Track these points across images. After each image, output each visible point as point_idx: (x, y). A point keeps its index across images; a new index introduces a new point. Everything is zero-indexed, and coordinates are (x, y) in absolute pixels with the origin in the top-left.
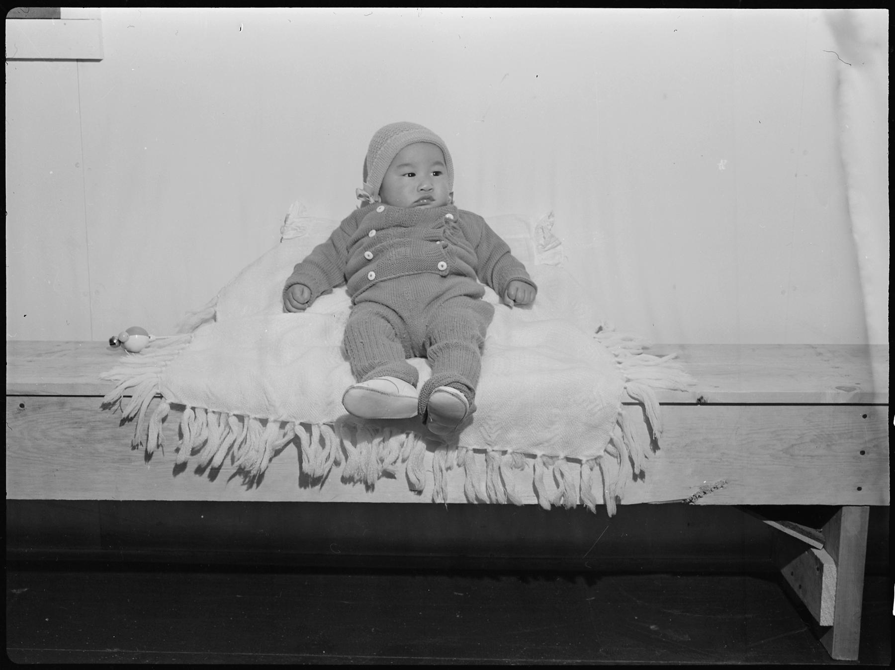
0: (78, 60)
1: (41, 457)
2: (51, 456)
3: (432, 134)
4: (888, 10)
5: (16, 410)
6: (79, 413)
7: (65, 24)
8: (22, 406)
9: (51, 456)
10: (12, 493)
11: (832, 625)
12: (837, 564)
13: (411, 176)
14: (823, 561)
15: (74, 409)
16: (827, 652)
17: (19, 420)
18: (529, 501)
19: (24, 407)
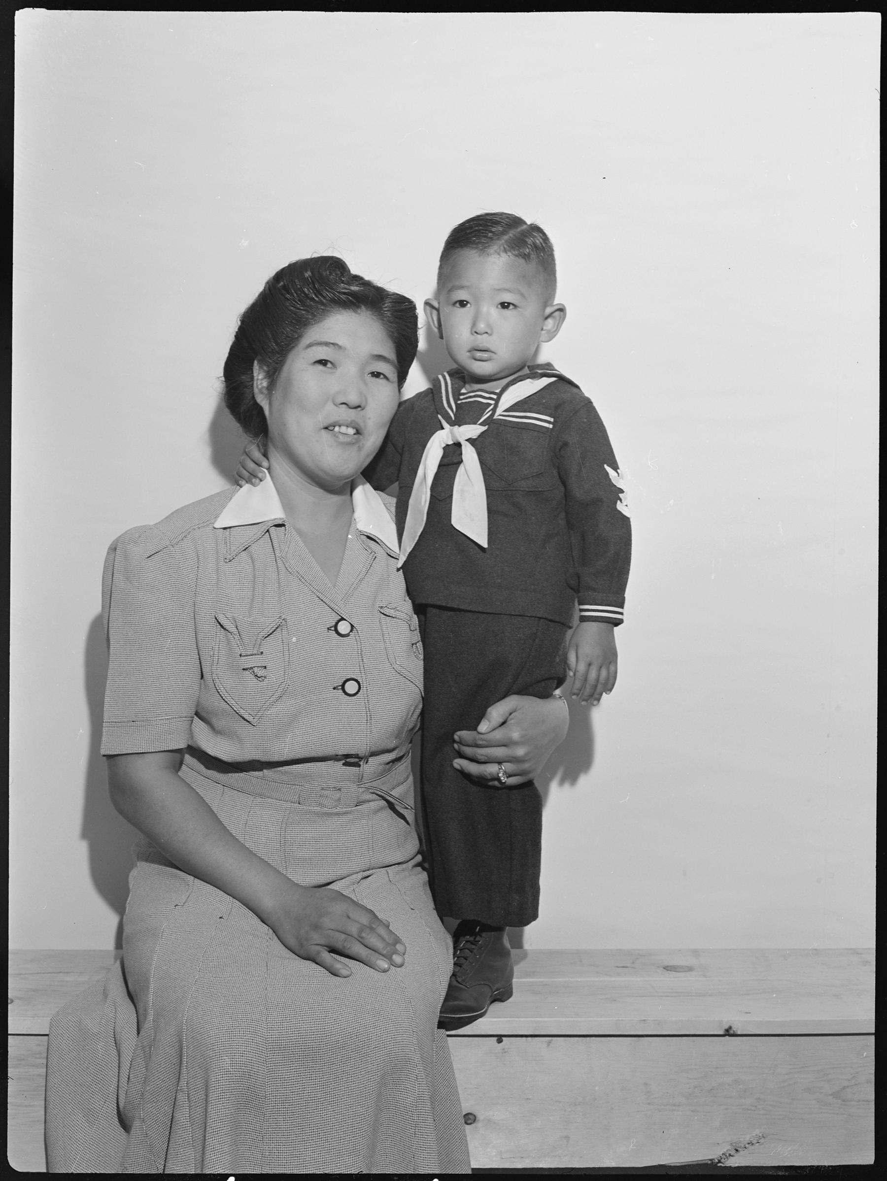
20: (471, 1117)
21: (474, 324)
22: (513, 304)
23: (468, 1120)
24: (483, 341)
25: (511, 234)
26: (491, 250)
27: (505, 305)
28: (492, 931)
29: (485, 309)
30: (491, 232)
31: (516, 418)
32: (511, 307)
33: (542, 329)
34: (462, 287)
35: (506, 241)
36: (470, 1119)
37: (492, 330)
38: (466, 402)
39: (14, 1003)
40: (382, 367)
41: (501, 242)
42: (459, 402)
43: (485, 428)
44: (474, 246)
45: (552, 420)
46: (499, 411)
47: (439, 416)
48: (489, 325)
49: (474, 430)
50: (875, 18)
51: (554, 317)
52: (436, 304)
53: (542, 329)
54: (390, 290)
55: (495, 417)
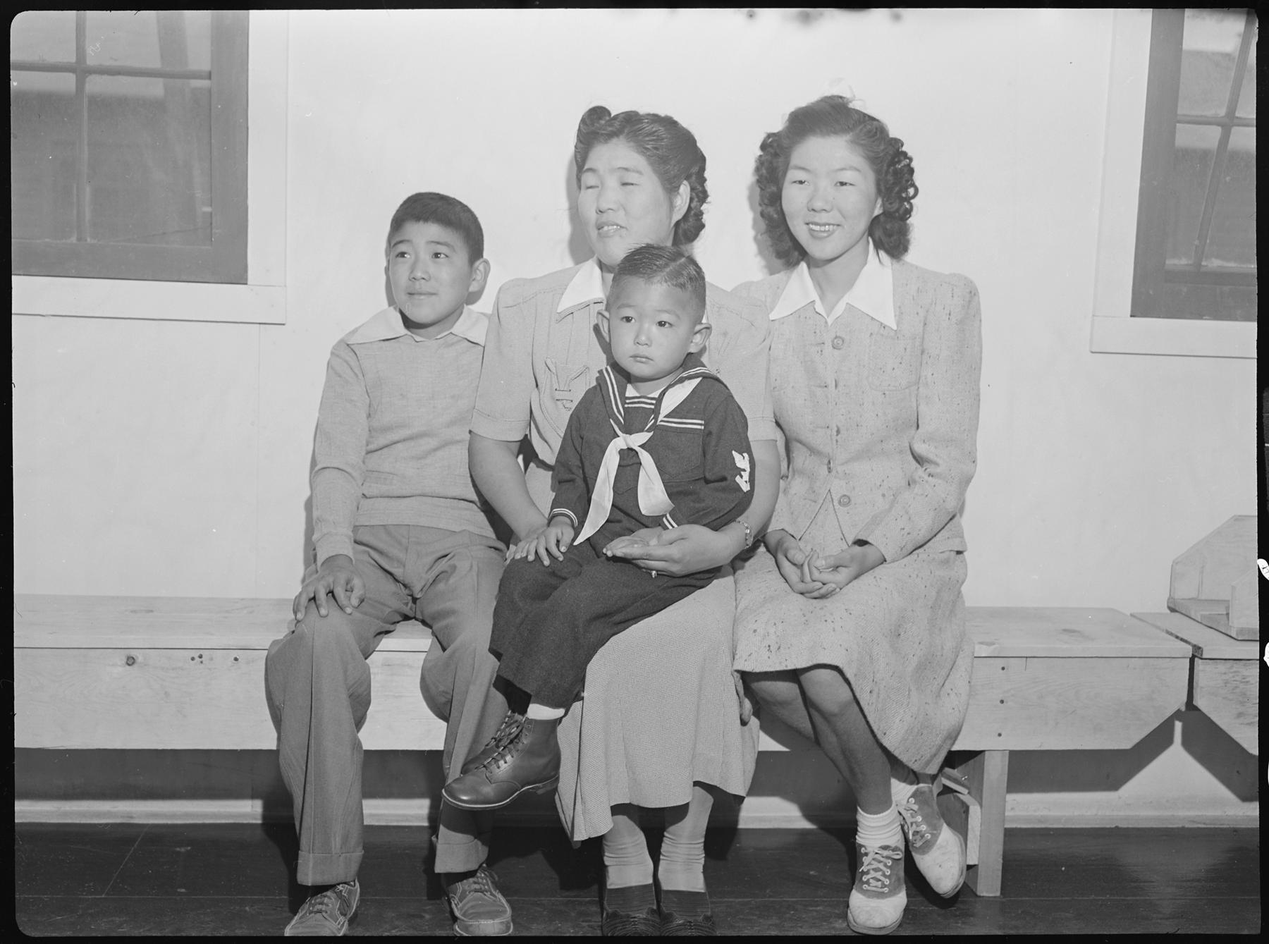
3: (393, 638)
4: (1257, 931)
11: (977, 863)
12: (981, 806)
14: (968, 804)
16: (972, 890)
21: (637, 337)
22: (669, 323)
24: (643, 350)
25: (673, 266)
26: (657, 279)
27: (661, 324)
28: (14, 898)
29: (646, 326)
30: (655, 265)
31: (675, 423)
32: (667, 325)
33: (692, 342)
34: (629, 306)
35: (667, 273)
37: (651, 343)
38: (632, 407)
41: (662, 274)
42: (626, 406)
43: (652, 433)
44: (642, 275)
45: (703, 422)
46: (661, 417)
47: (611, 421)
48: (649, 339)
49: (644, 437)
51: (702, 334)
52: (607, 314)
53: (692, 342)
55: (658, 423)
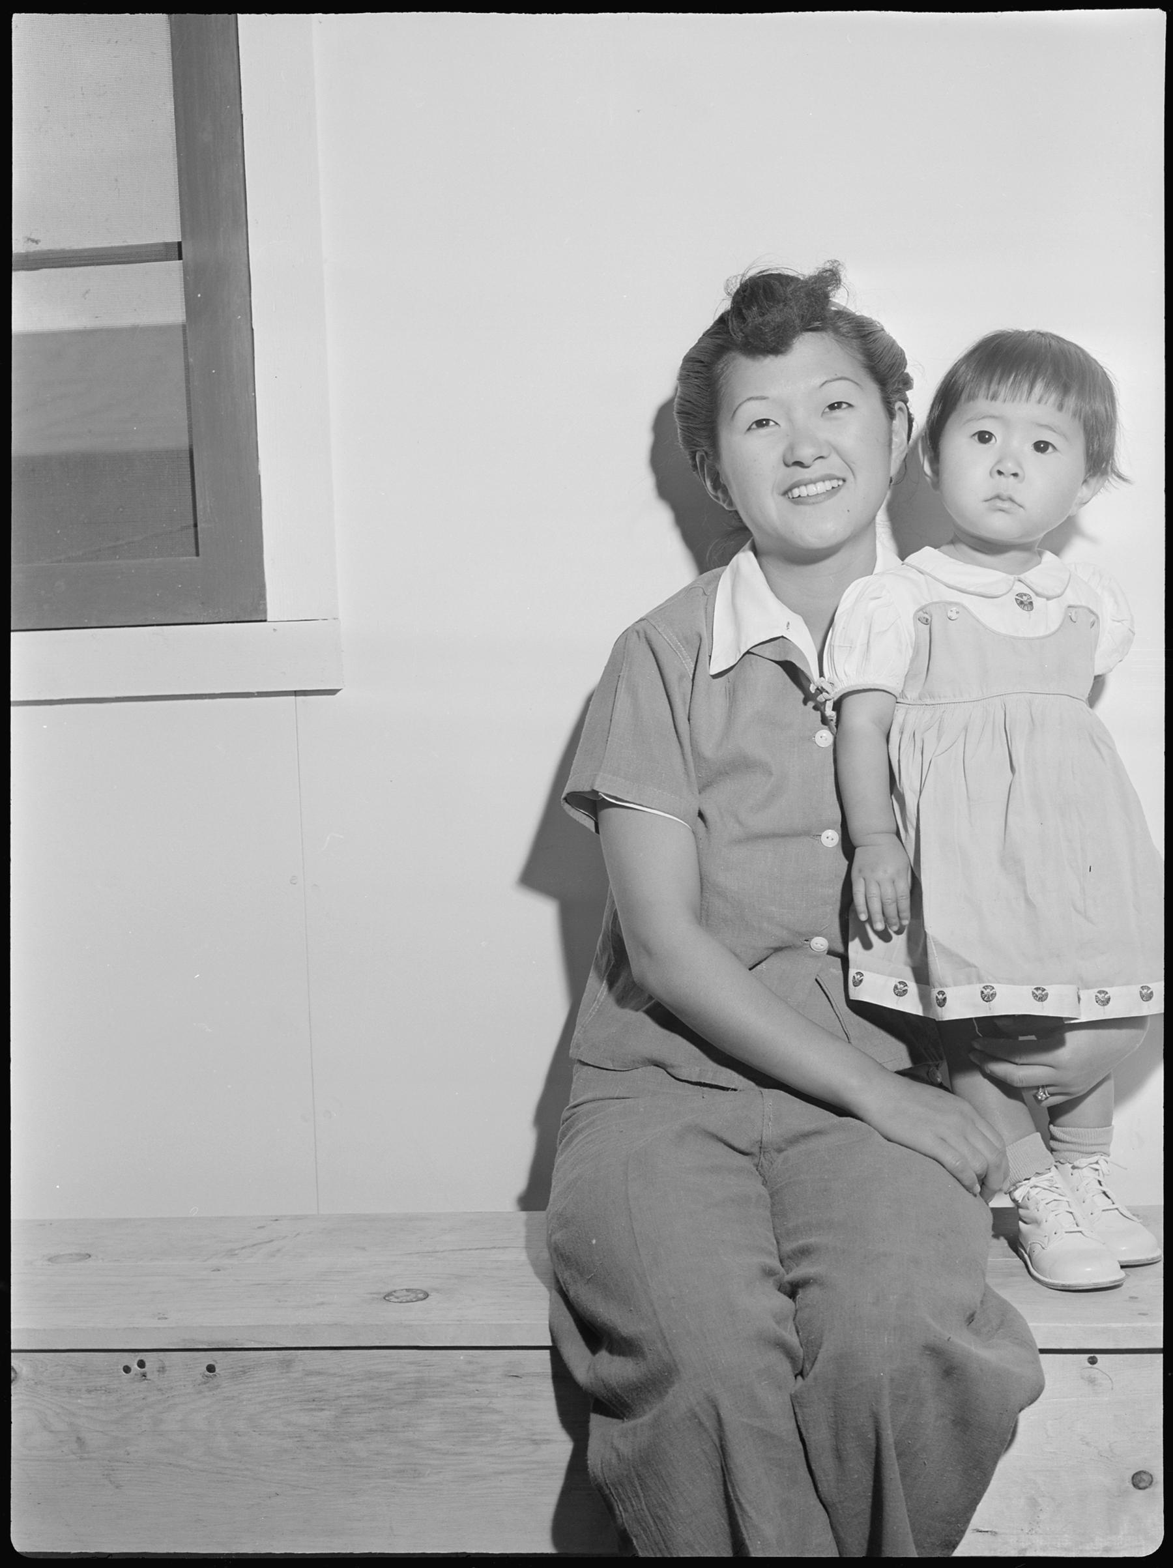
0: (296, 693)
1: (247, 1469)
2: (266, 1466)
5: (200, 1377)
6: (314, 1380)
7: (275, 630)
8: (211, 1369)
9: (266, 1466)
10: (541, 1544)
13: (834, 404)
15: (310, 1374)
17: (204, 1397)
18: (1098, 1553)
19: (214, 1371)
20: (1144, 1477)
23: (1140, 1482)
36: (1144, 1480)
39: (430, 1297)
40: (839, 391)
50: (1157, 17)
54: (1118, 465)
